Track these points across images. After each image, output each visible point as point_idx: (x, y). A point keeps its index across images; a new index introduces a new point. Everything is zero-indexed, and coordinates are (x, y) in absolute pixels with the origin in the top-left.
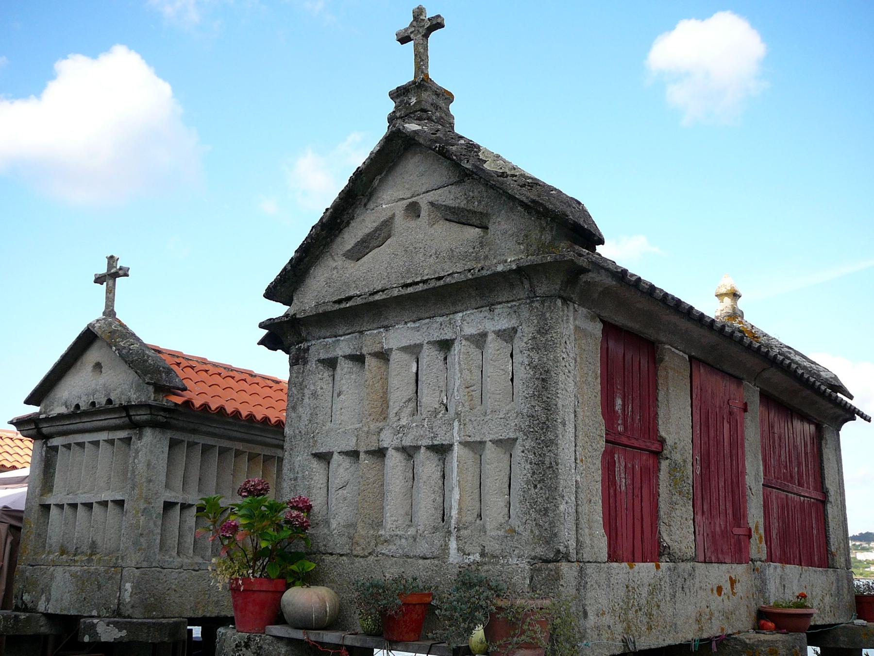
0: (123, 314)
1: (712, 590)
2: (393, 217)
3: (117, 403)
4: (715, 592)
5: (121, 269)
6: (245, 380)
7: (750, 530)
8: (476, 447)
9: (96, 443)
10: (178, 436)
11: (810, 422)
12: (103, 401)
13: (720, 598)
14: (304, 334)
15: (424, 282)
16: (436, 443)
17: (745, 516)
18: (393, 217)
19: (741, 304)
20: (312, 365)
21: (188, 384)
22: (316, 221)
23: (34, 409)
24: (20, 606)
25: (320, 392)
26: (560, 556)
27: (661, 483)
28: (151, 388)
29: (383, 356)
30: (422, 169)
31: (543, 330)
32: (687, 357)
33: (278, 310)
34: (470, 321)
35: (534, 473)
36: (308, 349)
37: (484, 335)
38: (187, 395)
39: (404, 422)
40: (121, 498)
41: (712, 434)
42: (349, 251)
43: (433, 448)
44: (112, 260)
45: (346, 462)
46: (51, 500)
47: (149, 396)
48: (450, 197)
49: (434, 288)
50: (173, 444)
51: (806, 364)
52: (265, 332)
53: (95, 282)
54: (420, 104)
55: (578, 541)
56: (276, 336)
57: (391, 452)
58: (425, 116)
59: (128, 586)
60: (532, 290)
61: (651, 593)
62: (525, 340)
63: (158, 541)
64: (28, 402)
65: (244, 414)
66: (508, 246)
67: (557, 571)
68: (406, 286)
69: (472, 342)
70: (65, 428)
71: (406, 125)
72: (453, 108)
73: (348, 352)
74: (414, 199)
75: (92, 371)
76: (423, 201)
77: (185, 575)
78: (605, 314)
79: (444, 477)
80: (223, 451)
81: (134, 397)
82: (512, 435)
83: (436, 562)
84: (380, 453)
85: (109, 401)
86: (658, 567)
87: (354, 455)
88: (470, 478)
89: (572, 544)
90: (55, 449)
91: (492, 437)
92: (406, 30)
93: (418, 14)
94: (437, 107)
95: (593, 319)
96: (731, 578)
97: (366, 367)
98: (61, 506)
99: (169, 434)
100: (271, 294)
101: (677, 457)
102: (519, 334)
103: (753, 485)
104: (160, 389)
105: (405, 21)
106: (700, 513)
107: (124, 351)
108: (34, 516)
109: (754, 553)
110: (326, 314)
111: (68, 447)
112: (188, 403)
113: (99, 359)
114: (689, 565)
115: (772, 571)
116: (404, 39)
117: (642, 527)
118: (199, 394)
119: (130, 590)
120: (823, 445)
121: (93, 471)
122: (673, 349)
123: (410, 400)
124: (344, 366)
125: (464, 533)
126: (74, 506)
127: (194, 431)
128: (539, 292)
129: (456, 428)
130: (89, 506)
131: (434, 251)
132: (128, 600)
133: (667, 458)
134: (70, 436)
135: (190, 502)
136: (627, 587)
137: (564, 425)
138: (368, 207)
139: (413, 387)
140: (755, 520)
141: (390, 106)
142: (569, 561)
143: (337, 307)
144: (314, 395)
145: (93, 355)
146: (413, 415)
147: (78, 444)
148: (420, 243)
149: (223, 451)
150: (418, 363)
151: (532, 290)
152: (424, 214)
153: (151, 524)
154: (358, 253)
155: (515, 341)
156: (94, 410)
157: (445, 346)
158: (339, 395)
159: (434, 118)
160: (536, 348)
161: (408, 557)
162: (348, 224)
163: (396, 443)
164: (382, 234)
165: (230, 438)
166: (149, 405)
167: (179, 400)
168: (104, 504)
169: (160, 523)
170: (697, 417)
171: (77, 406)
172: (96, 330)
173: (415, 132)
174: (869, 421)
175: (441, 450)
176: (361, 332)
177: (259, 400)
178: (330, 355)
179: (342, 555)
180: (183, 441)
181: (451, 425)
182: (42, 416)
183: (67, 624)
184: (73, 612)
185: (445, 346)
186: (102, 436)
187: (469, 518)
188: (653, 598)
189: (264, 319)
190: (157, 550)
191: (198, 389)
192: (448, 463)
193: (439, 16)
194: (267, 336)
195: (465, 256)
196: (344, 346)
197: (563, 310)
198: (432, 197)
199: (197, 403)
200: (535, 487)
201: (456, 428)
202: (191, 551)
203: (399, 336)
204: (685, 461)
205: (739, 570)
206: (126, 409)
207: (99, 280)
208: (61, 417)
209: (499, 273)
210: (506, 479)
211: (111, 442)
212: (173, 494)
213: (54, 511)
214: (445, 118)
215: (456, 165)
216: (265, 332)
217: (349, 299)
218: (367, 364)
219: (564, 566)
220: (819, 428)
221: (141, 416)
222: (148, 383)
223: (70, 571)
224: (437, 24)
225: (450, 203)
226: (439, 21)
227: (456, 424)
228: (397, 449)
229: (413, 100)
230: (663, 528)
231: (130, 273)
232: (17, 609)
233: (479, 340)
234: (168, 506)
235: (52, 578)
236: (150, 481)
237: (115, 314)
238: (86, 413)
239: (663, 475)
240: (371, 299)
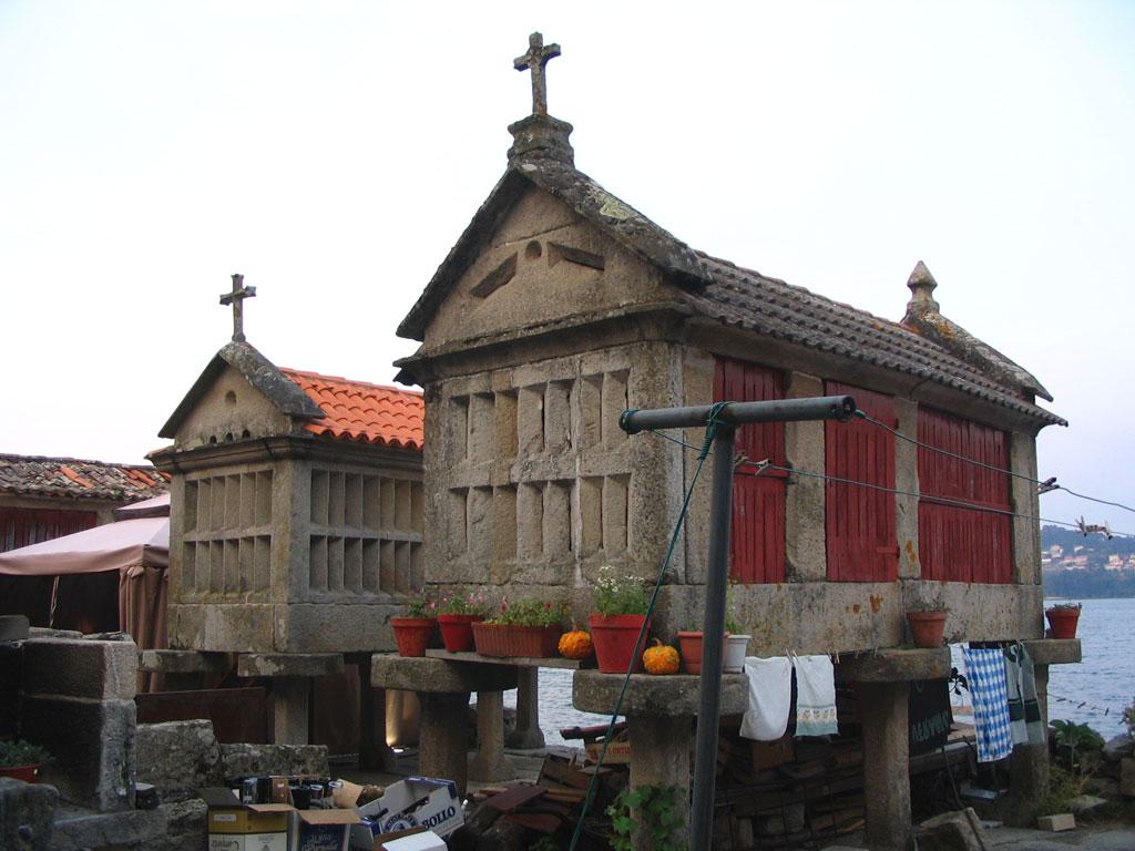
0: (252, 337)
1: (847, 608)
2: (516, 255)
3: (254, 436)
4: (851, 610)
5: (247, 288)
6: (387, 399)
7: (899, 549)
8: (596, 481)
9: (236, 478)
10: (320, 466)
11: (994, 429)
12: (240, 433)
13: (857, 616)
14: (436, 373)
15: (544, 325)
16: (561, 477)
17: (893, 535)
18: (516, 255)
19: (936, 295)
20: (445, 403)
21: (328, 409)
22: (442, 261)
23: (168, 443)
24: (175, 644)
25: (454, 429)
26: (666, 580)
27: (788, 508)
28: (289, 419)
29: (512, 394)
30: (541, 207)
31: (652, 373)
32: (820, 380)
33: (410, 348)
34: (592, 363)
35: (645, 505)
36: (441, 387)
37: (601, 375)
38: (328, 422)
39: (532, 458)
40: (266, 533)
41: (852, 453)
42: (475, 288)
43: (557, 483)
44: (237, 279)
45: (481, 497)
46: (195, 536)
47: (290, 428)
48: (569, 238)
49: (553, 331)
50: (316, 476)
51: (1002, 364)
52: (399, 370)
53: (222, 302)
54: (541, 137)
55: (686, 565)
56: (409, 370)
57: (520, 487)
58: (542, 153)
59: (282, 622)
60: (641, 333)
61: (771, 612)
62: (637, 381)
63: (308, 576)
64: (162, 435)
65: (387, 439)
66: (621, 290)
67: (666, 592)
68: (530, 328)
69: (590, 381)
70: (202, 462)
71: (524, 166)
72: (573, 139)
73: (479, 390)
74: (535, 238)
75: (226, 401)
76: (543, 240)
77: (337, 610)
78: (715, 350)
79: (569, 509)
80: (368, 481)
81: (272, 429)
82: (626, 471)
83: (564, 588)
84: (511, 488)
85: (246, 433)
86: (779, 588)
87: (488, 489)
88: (592, 511)
89: (681, 569)
90: (194, 484)
91: (609, 472)
92: (523, 57)
93: (536, 39)
94: (553, 141)
95: (704, 356)
96: (872, 598)
97: (496, 405)
98: (206, 544)
99: (311, 465)
100: (405, 331)
101: (806, 481)
102: (631, 375)
103: (905, 503)
104: (297, 418)
105: (523, 48)
106: (834, 534)
107: (259, 380)
108: (179, 554)
109: (903, 570)
110: (455, 354)
111: (207, 481)
112: (328, 433)
113: (231, 388)
114: (818, 585)
115: (928, 588)
116: (520, 66)
117: (765, 551)
118: (340, 420)
119: (284, 626)
120: (1012, 453)
121: (232, 511)
122: (803, 375)
123: (536, 437)
124: (476, 406)
125: (588, 561)
126: (219, 543)
127: (336, 461)
128: (647, 336)
129: (578, 464)
130: (234, 542)
131: (554, 292)
132: (282, 635)
133: (793, 483)
134: (208, 471)
135: (338, 535)
136: (743, 606)
137: (671, 460)
138: (493, 244)
139: (539, 424)
140: (907, 539)
141: (509, 141)
142: (678, 584)
143: (465, 347)
144: (450, 431)
145: (227, 383)
146: (541, 451)
147: (216, 478)
148: (542, 289)
149: (368, 481)
150: (543, 400)
151: (641, 333)
152: (545, 253)
153: (299, 559)
154: (484, 291)
155: (630, 381)
156: (230, 443)
157: (567, 385)
158: (472, 432)
159: (552, 155)
160: (645, 389)
161: (539, 583)
162: (474, 261)
163: (525, 478)
164: (505, 272)
165: (373, 466)
166: (288, 437)
167: (319, 430)
168: (250, 540)
169: (308, 557)
170: (832, 438)
171: (213, 439)
172: (228, 358)
173: (530, 172)
174: (1067, 425)
175: (566, 485)
176: (490, 371)
177: (402, 420)
178: (463, 393)
179: (481, 584)
180: (325, 472)
181: (573, 461)
182: (179, 451)
183: (218, 660)
184: (229, 649)
185: (567, 385)
186: (242, 470)
187: (592, 547)
188: (772, 617)
189: (398, 358)
190: (307, 585)
191: (338, 413)
192: (573, 499)
193: (554, 45)
194: (401, 373)
195: (582, 299)
196: (474, 385)
197: (670, 353)
198: (551, 237)
199: (338, 431)
200: (647, 518)
201: (578, 464)
202: (342, 585)
203: (524, 376)
204: (816, 485)
205: (883, 589)
206: (265, 441)
207: (225, 300)
208: (198, 451)
209: (610, 318)
210: (623, 511)
211: (251, 476)
212: (319, 527)
213: (199, 549)
214: (564, 151)
215: (570, 207)
216: (399, 370)
217: (476, 339)
218: (496, 402)
219: (672, 588)
220: (1008, 437)
221: (281, 449)
222: (286, 414)
223: (222, 609)
224: (554, 51)
225: (567, 244)
226: (556, 49)
227: (578, 460)
228: (526, 484)
229: (531, 137)
230: (789, 551)
231: (257, 292)
232: (173, 647)
233: (597, 379)
234: (315, 540)
235: (205, 616)
236: (294, 515)
237: (244, 338)
238: (223, 447)
239: (790, 499)
240: (497, 340)
